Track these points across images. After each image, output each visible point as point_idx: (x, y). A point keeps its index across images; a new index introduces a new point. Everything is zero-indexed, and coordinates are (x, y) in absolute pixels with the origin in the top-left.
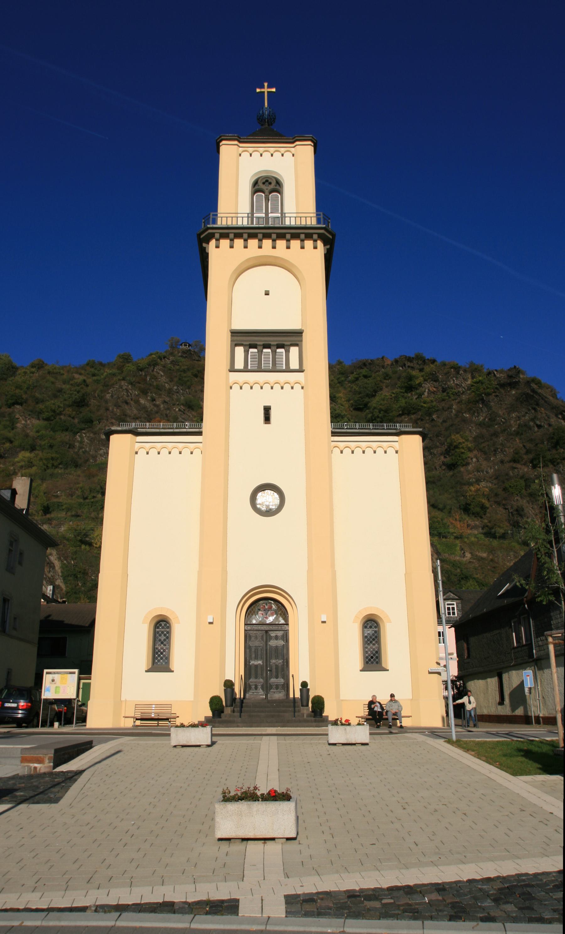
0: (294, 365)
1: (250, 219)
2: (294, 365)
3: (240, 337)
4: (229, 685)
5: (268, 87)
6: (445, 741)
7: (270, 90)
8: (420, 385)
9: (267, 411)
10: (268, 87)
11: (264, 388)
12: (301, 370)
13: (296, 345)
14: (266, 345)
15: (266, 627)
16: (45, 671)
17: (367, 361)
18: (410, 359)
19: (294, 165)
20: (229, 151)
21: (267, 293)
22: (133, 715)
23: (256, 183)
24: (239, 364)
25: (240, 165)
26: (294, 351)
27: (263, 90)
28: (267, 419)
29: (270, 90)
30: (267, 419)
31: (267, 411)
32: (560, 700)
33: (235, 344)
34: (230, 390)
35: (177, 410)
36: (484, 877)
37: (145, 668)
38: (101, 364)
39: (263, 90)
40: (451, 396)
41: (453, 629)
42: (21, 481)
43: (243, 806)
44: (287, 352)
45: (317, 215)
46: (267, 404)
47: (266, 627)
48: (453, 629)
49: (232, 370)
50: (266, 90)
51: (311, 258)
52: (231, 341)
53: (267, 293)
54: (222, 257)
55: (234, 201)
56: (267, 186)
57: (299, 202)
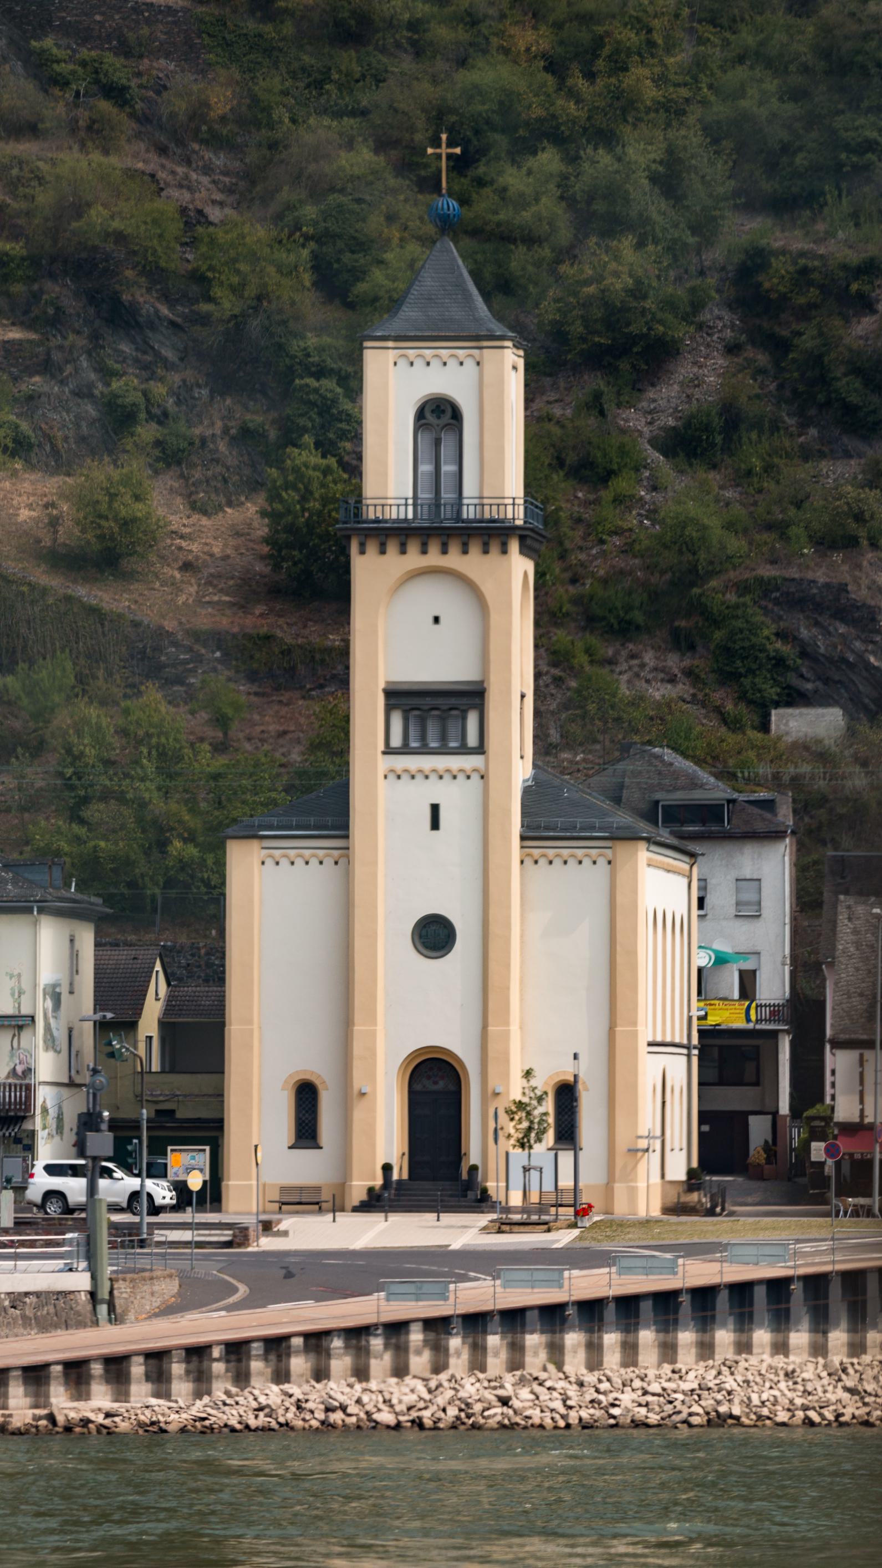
0: (472, 741)
2: (472, 741)
3: (397, 697)
4: (387, 1168)
5: (450, 156)
6: (766, 1142)
7: (450, 151)
9: (435, 809)
10: (450, 156)
11: (442, 780)
12: (480, 749)
13: (473, 707)
14: (440, 714)
15: (436, 1086)
16: (169, 1148)
19: (496, 387)
23: (420, 415)
24: (396, 741)
25: (394, 384)
27: (444, 145)
28: (435, 825)
29: (450, 151)
30: (435, 825)
31: (435, 809)
32: (373, 1019)
34: (388, 788)
37: (286, 1145)
39: (444, 145)
40: (645, 200)
43: (15, 1437)
44: (464, 719)
45: (525, 502)
46: (435, 832)
47: (436, 1086)
49: (389, 751)
50: (444, 151)
53: (437, 620)
55: (391, 475)
56: (439, 417)
57: (499, 471)
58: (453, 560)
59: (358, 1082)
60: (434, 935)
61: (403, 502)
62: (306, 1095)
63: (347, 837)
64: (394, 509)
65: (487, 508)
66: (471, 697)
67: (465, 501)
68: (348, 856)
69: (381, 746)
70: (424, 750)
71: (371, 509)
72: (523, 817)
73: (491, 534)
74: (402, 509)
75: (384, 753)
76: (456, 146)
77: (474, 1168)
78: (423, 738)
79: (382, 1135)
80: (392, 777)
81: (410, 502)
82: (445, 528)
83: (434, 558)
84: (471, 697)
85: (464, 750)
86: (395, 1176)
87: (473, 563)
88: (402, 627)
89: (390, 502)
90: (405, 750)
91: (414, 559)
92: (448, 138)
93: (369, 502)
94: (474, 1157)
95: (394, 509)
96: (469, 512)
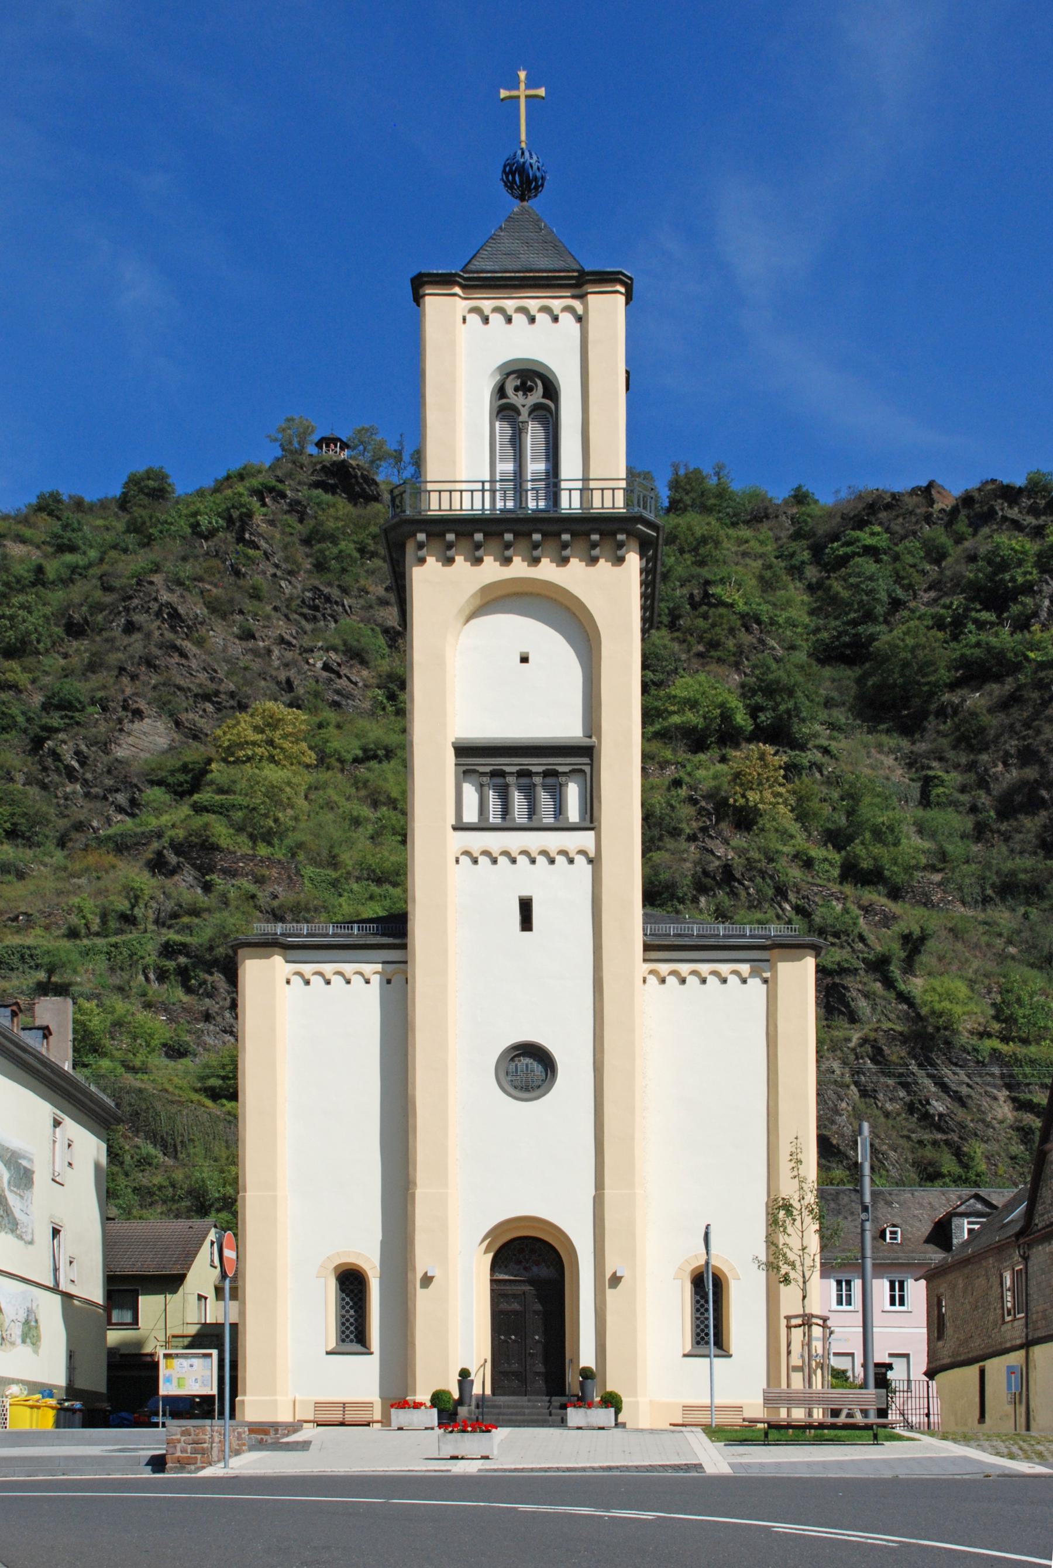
0: (573, 813)
1: (487, 494)
2: (573, 813)
4: (464, 1374)
8: (1028, 589)
9: (526, 906)
14: (522, 776)
15: (532, 1273)
17: (880, 497)
18: (1010, 494)
20: (445, 314)
21: (524, 660)
22: (311, 1418)
24: (471, 816)
26: (573, 792)
27: (522, 86)
28: (526, 923)
30: (526, 923)
31: (526, 906)
33: (465, 773)
34: (460, 878)
35: (319, 664)
36: (488, 1356)
38: (79, 504)
39: (522, 86)
41: (923, 1282)
42: (50, 1006)
46: (525, 893)
47: (532, 1273)
48: (923, 1282)
49: (460, 827)
51: (613, 590)
52: (456, 765)
53: (524, 660)
54: (439, 585)
55: (462, 458)
56: (527, 396)
58: (547, 570)
59: (423, 1262)
60: (529, 1067)
61: (479, 486)
62: (351, 1283)
63: (404, 947)
64: (466, 496)
65: (597, 494)
66: (581, 756)
67: (563, 485)
68: (405, 972)
69: (452, 820)
70: (508, 826)
71: (434, 496)
72: (645, 923)
73: (593, 534)
74: (478, 495)
75: (455, 828)
76: (538, 87)
77: (587, 1374)
78: (506, 810)
79: (458, 1331)
80: (465, 860)
81: (487, 486)
82: (532, 527)
83: (519, 568)
84: (581, 756)
85: (563, 827)
86: (477, 1390)
87: (575, 576)
88: (482, 666)
89: (459, 486)
90: (482, 827)
91: (491, 570)
92: (527, 77)
93: (430, 486)
94: (587, 1358)
95: (466, 496)
96: (570, 502)
